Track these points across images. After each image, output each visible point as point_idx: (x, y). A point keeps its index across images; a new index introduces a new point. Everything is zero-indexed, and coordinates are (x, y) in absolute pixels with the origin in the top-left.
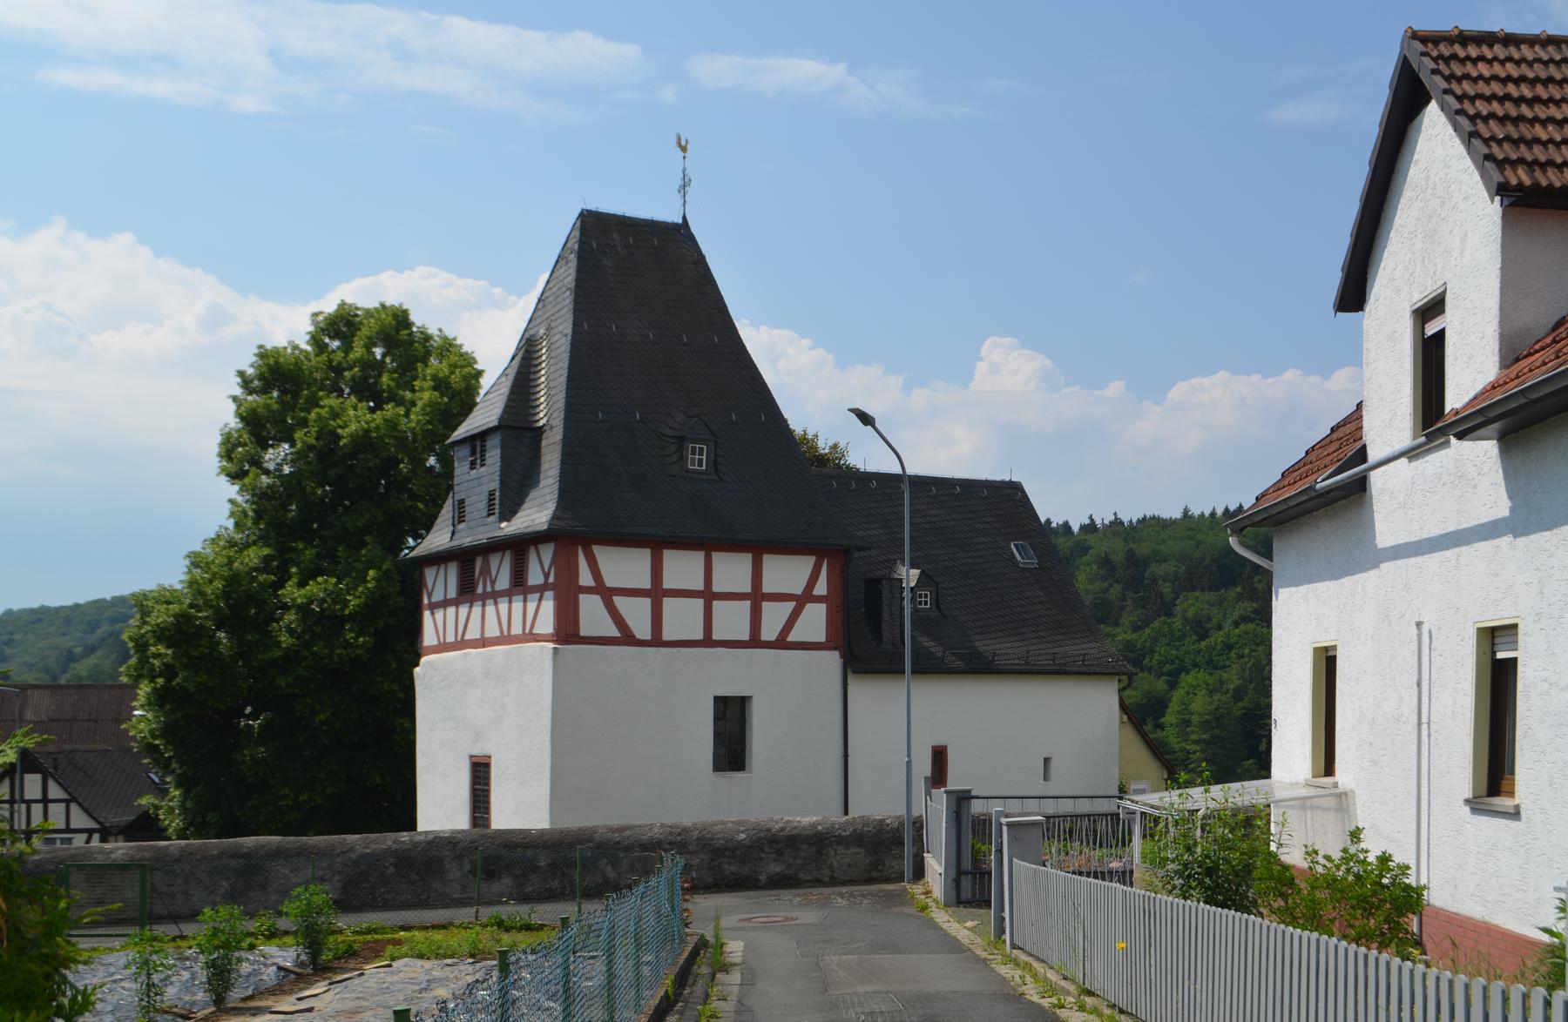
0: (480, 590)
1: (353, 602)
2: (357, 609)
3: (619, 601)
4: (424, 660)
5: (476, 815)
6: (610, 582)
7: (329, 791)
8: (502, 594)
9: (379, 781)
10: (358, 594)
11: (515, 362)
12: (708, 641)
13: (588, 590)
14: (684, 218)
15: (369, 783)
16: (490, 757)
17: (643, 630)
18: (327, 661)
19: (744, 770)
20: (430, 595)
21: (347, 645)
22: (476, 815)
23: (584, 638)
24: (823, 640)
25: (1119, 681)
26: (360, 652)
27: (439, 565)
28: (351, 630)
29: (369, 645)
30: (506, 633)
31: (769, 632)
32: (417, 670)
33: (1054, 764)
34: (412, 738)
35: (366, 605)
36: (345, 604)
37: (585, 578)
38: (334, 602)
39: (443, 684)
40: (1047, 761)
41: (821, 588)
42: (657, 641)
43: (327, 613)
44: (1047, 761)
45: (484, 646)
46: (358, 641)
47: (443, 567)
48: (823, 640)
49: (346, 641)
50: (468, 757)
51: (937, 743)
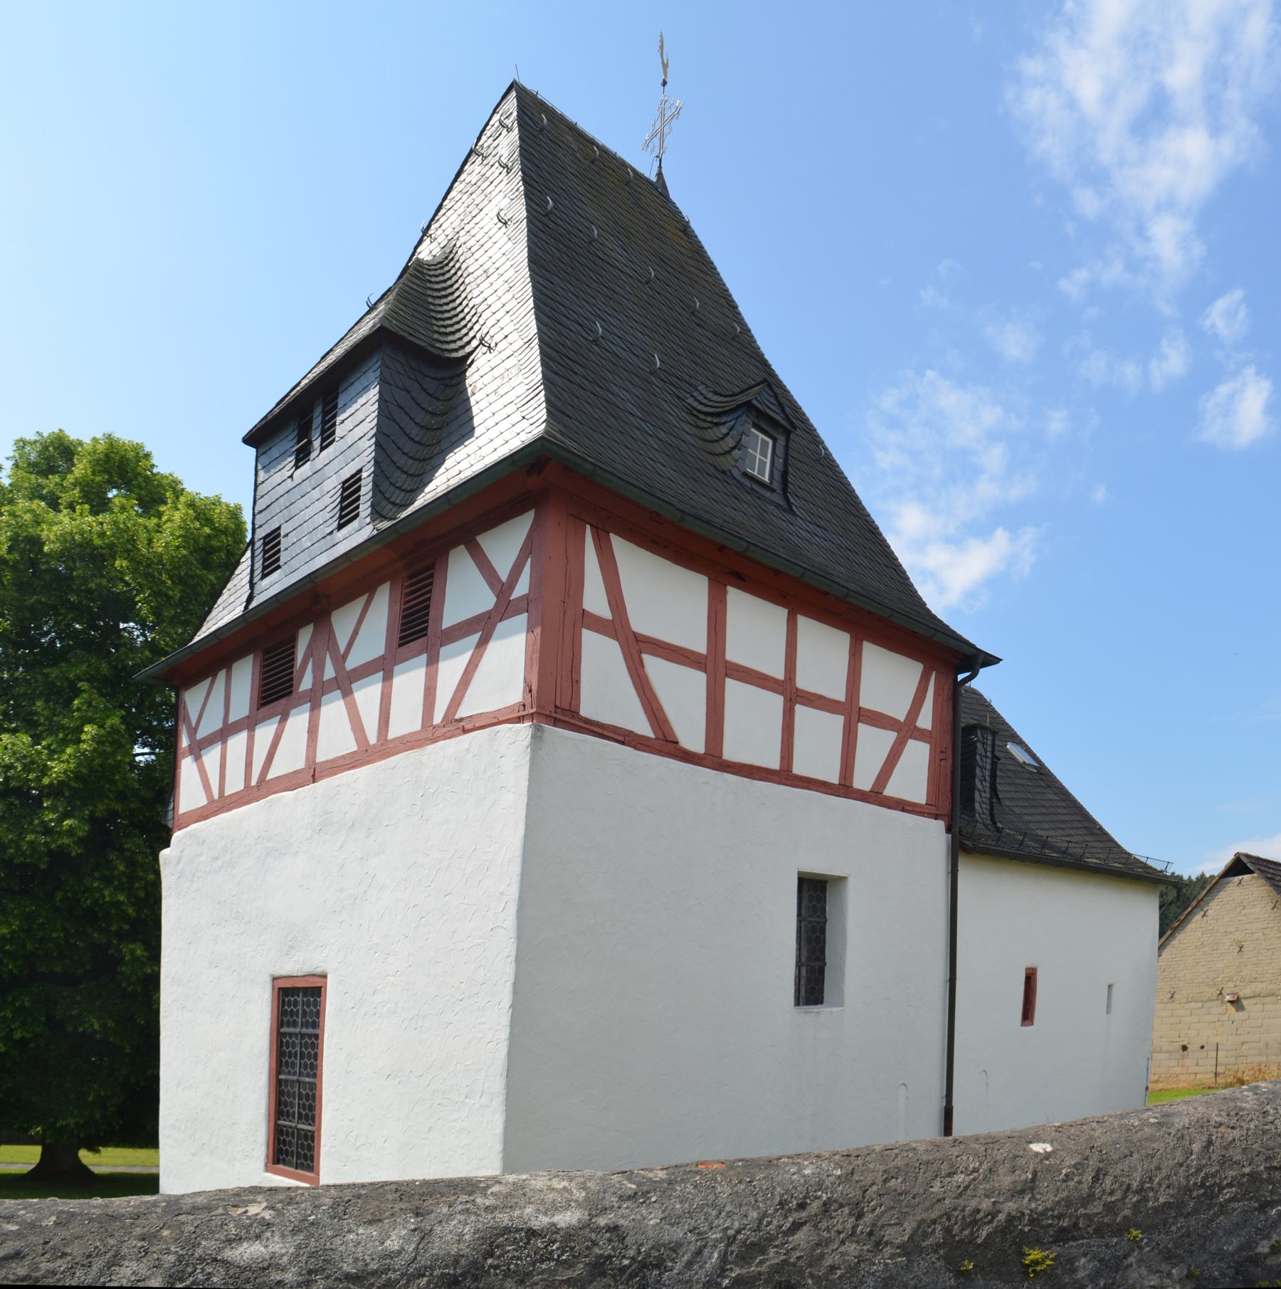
0: (306, 683)
1: (57, 768)
2: (62, 777)
3: (654, 666)
4: (177, 836)
5: (282, 1077)
6: (640, 623)
7: (17, 1035)
8: (365, 671)
9: (96, 1026)
10: (65, 757)
11: (351, 381)
12: (784, 776)
13: (598, 625)
14: (660, 175)
15: (81, 1030)
16: (324, 976)
17: (692, 737)
18: (12, 851)
19: (822, 1003)
20: (193, 731)
21: (47, 831)
22: (282, 1077)
23: (587, 721)
24: (923, 801)
25: (1161, 895)
26: (66, 841)
27: (215, 676)
28: (53, 809)
29: (80, 834)
30: (372, 739)
31: (863, 780)
32: (164, 854)
33: (1115, 989)
34: (157, 969)
35: (78, 776)
36: (45, 770)
37: (595, 600)
38: (27, 769)
39: (219, 863)
40: (1110, 987)
41: (925, 720)
42: (712, 759)
43: (13, 784)
44: (1110, 987)
45: (314, 779)
46: (62, 826)
47: (222, 675)
48: (923, 801)
49: (44, 825)
50: (269, 980)
51: (1030, 965)
